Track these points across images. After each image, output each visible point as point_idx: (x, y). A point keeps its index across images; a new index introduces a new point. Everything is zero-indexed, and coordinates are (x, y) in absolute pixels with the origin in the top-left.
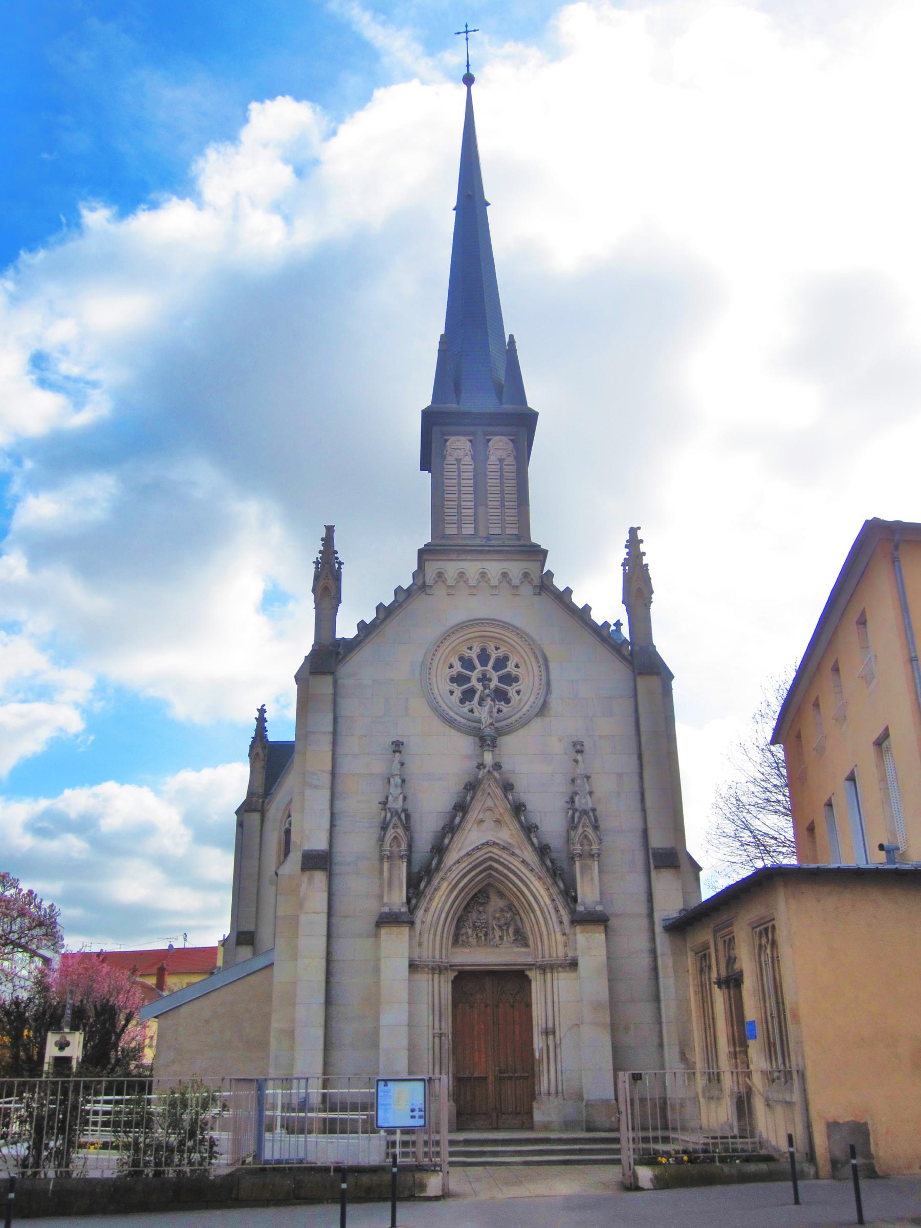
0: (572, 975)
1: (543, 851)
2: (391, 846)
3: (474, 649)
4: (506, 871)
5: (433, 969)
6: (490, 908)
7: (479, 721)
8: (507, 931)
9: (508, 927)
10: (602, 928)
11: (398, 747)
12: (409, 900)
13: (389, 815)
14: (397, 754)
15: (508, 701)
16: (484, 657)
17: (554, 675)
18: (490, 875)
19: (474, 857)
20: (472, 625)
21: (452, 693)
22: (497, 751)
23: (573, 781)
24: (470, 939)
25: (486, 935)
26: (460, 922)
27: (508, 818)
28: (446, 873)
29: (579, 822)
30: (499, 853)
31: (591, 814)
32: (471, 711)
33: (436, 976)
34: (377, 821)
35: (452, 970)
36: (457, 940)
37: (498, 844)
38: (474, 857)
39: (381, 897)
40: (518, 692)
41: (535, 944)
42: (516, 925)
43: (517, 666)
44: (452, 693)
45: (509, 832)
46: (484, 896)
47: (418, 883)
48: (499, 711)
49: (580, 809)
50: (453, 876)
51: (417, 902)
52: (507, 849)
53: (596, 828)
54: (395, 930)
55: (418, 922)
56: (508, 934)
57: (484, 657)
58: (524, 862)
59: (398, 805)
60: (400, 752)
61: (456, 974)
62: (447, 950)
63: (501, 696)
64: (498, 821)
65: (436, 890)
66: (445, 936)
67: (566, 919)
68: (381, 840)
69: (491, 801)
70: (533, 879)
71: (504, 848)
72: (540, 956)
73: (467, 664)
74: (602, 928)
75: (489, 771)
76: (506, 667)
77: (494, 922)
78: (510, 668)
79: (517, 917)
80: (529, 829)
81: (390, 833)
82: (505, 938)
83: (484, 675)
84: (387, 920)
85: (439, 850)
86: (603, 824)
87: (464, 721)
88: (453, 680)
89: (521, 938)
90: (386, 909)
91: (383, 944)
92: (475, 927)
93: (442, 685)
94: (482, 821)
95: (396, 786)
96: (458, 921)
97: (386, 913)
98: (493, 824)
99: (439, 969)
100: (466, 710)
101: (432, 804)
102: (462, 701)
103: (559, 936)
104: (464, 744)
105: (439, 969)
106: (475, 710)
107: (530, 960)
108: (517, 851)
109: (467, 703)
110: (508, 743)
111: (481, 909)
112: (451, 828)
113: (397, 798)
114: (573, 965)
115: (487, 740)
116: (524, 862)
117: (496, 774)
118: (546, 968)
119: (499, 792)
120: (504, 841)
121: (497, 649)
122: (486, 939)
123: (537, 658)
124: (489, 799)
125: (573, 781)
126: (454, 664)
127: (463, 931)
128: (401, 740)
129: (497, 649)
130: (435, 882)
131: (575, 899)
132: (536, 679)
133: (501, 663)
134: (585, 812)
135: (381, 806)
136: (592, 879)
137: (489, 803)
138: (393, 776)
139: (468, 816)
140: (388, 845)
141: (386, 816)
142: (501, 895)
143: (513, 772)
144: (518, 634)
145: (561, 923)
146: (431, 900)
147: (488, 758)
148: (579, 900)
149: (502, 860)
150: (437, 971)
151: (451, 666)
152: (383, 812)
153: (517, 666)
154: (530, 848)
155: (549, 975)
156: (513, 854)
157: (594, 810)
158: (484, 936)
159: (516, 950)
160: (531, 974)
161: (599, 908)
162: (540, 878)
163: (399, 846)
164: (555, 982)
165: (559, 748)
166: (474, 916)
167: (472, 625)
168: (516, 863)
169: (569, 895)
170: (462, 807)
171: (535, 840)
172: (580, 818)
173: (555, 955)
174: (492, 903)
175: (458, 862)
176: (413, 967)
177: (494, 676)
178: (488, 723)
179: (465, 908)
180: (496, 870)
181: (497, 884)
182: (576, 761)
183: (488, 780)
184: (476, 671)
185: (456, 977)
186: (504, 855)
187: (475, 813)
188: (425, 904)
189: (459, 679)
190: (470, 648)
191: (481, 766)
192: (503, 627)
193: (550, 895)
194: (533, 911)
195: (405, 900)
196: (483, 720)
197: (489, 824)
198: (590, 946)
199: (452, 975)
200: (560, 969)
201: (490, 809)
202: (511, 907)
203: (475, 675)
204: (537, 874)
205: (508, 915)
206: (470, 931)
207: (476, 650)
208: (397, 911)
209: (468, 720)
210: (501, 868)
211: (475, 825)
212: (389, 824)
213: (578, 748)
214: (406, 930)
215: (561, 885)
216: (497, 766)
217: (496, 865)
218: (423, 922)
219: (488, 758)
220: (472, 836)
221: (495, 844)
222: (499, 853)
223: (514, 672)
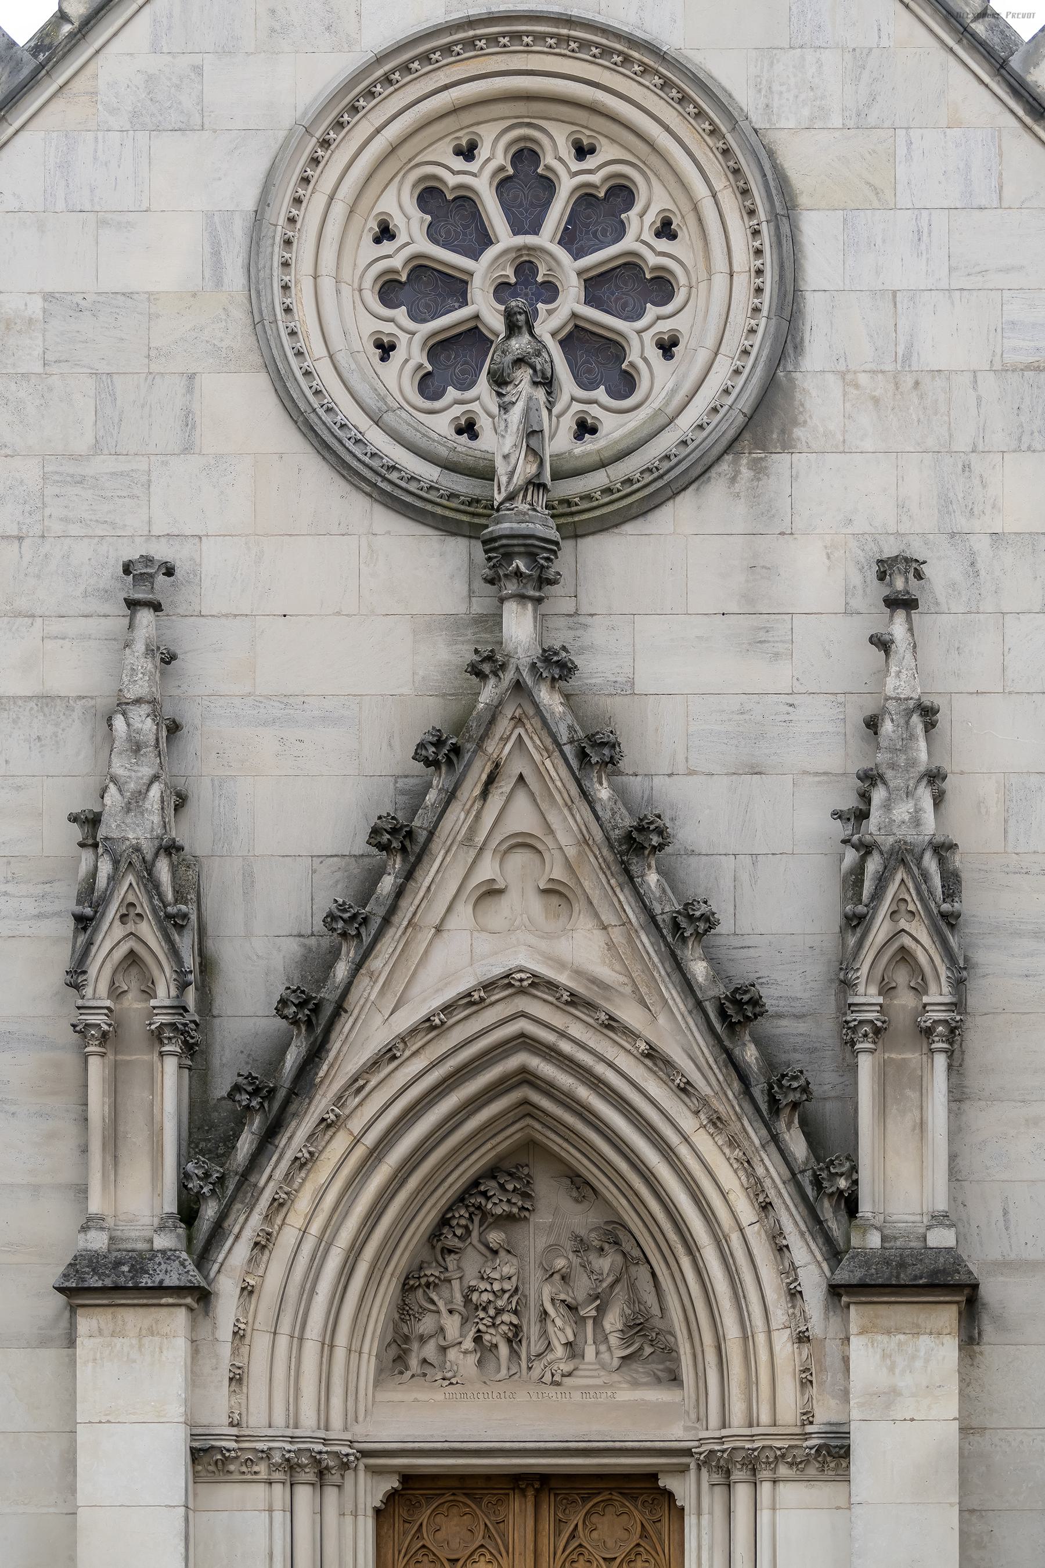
0: (823, 1492)
1: (736, 1012)
2: (116, 993)
3: (483, 152)
4: (583, 1093)
5: (291, 1467)
6: (534, 1239)
7: (486, 473)
8: (597, 1321)
9: (601, 1310)
10: (947, 1316)
11: (146, 586)
12: (188, 1212)
13: (105, 868)
14: (145, 616)
15: (625, 384)
16: (526, 184)
17: (820, 268)
18: (526, 1110)
19: (456, 1036)
20: (470, 43)
21: (385, 349)
22: (559, 600)
23: (872, 724)
24: (452, 1354)
25: (515, 1337)
26: (414, 1289)
27: (594, 882)
28: (339, 1100)
29: (878, 894)
30: (557, 1020)
31: (930, 863)
32: (468, 429)
33: (304, 1495)
34: (66, 901)
35: (375, 1471)
36: (398, 1355)
37: (551, 986)
38: (456, 1036)
39: (82, 1191)
40: (667, 347)
41: (700, 1377)
42: (634, 1299)
43: (666, 230)
44: (385, 349)
45: (599, 936)
46: (510, 1180)
47: (238, 1128)
48: (585, 428)
49: (887, 842)
50: (370, 1115)
51: (223, 1216)
52: (590, 1006)
53: (946, 922)
54: (133, 1319)
55: (226, 1289)
56: (601, 1337)
57: (526, 184)
58: (653, 1056)
59: (139, 830)
60: (156, 607)
61: (393, 1483)
62: (351, 1392)
63: (598, 356)
64: (553, 892)
65: (300, 1164)
66: (342, 1338)
67: (813, 1278)
68: (76, 976)
69: (532, 809)
70: (688, 1122)
71: (575, 1000)
72: (714, 1419)
73: (451, 212)
74: (947, 1316)
75: (518, 686)
76: (620, 231)
77: (547, 1291)
78: (637, 235)
79: (642, 1273)
80: (685, 927)
81: (111, 940)
82: (590, 1351)
83: (525, 268)
84: (101, 1283)
85: (312, 1013)
86: (973, 903)
87: (430, 472)
88: (390, 290)
89: (650, 1348)
90: (97, 1241)
91: (84, 1373)
92: (471, 1307)
93: (340, 315)
94: (491, 892)
95: (137, 748)
96: (407, 1287)
97: (96, 1255)
98: (536, 905)
99: (315, 1467)
100: (442, 425)
101: (281, 820)
102: (429, 386)
103: (783, 1342)
104: (433, 571)
105: (315, 1467)
106: (484, 423)
107: (676, 1432)
108: (630, 1015)
109: (452, 393)
110: (612, 569)
111: (495, 1237)
112: (356, 924)
113: (141, 795)
114: (833, 1454)
115: (515, 544)
116: (653, 1056)
117: (548, 698)
118: (736, 1465)
119: (556, 771)
120: (578, 973)
121: (582, 151)
122: (514, 1353)
123: (745, 192)
124: (521, 800)
125: (872, 724)
126: (398, 221)
127: (426, 1325)
128: (162, 552)
129: (582, 151)
130: (297, 1136)
131: (850, 1204)
132: (742, 284)
133: (603, 208)
134: (902, 856)
135: (76, 832)
136: (922, 1125)
137: (522, 817)
138: (122, 706)
139: (426, 876)
140: (103, 988)
141: (94, 874)
142: (580, 1186)
143: (628, 689)
144: (667, 84)
145: (794, 1294)
146: (278, 1205)
147: (519, 629)
148: (865, 1208)
149: (566, 1047)
150: (310, 1476)
151: (385, 233)
152: (87, 857)
153: (666, 230)
154: (678, 1003)
155: (742, 1493)
156: (611, 1025)
157: (942, 849)
158: (504, 1335)
159: (626, 1395)
160: (683, 1489)
161: (941, 1238)
162: (717, 1122)
163: (149, 992)
164: (764, 1516)
165: (821, 583)
166: (470, 1265)
167: (470, 43)
168: (624, 1062)
169: (829, 1190)
170: (400, 839)
171: (699, 970)
172: (882, 882)
173: (765, 1418)
174: (542, 1218)
175: (389, 1055)
176: (207, 1459)
177: (569, 271)
178: (518, 479)
179: (435, 1235)
180: (548, 1088)
181: (555, 1143)
182: (883, 644)
183: (518, 721)
184: (490, 253)
185: (391, 1497)
186: (576, 1030)
187: (444, 873)
188: (256, 1219)
189: (420, 287)
190: (467, 152)
191: (486, 664)
192: (607, 52)
193: (756, 1190)
194: (692, 1249)
195: (170, 1205)
196: (502, 469)
197: (522, 904)
198: (901, 1380)
199: (369, 1491)
200: (783, 1470)
201: (524, 843)
202: (614, 1234)
203: (483, 271)
204: (705, 1102)
205: (606, 1264)
206: (452, 1325)
207: (494, 153)
208: (141, 1246)
209: (449, 466)
210: (564, 1080)
211: (464, 911)
212: (104, 900)
213: (899, 586)
214: (176, 1320)
215: (798, 1146)
216: (557, 666)
217: (546, 1069)
218: (248, 1291)
219: (519, 629)
220: (454, 948)
221: (538, 983)
222: (557, 1020)
223: (655, 255)
